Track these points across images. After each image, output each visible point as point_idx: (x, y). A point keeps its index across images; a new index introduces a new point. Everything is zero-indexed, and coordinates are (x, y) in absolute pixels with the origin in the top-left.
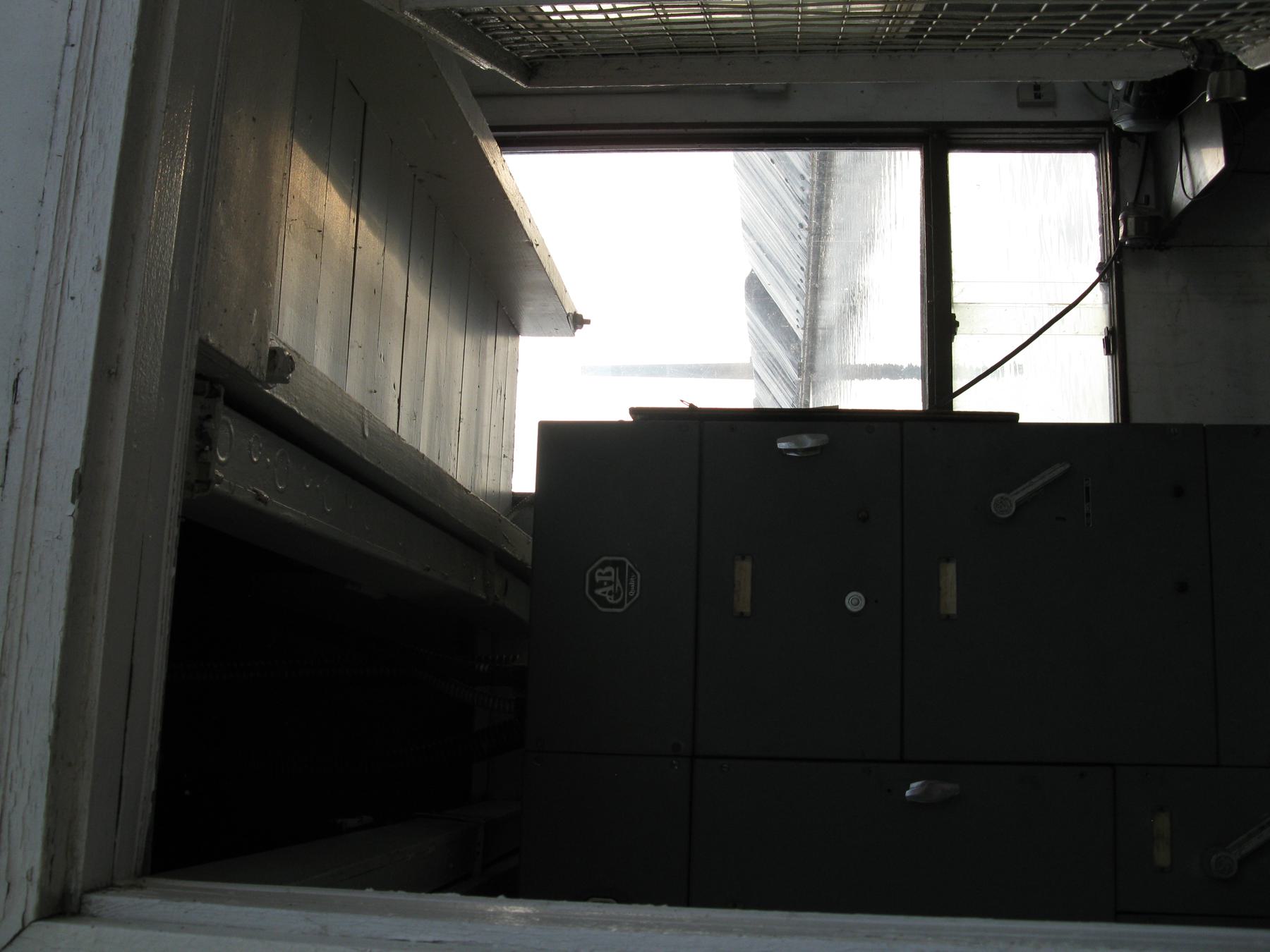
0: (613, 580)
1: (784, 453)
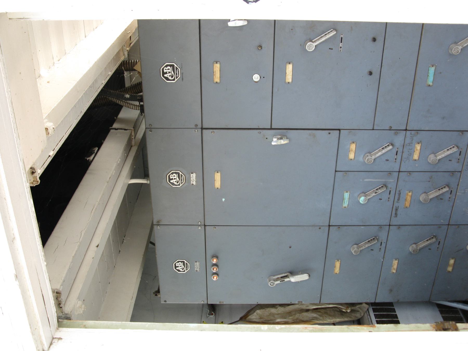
0: (176, 178)
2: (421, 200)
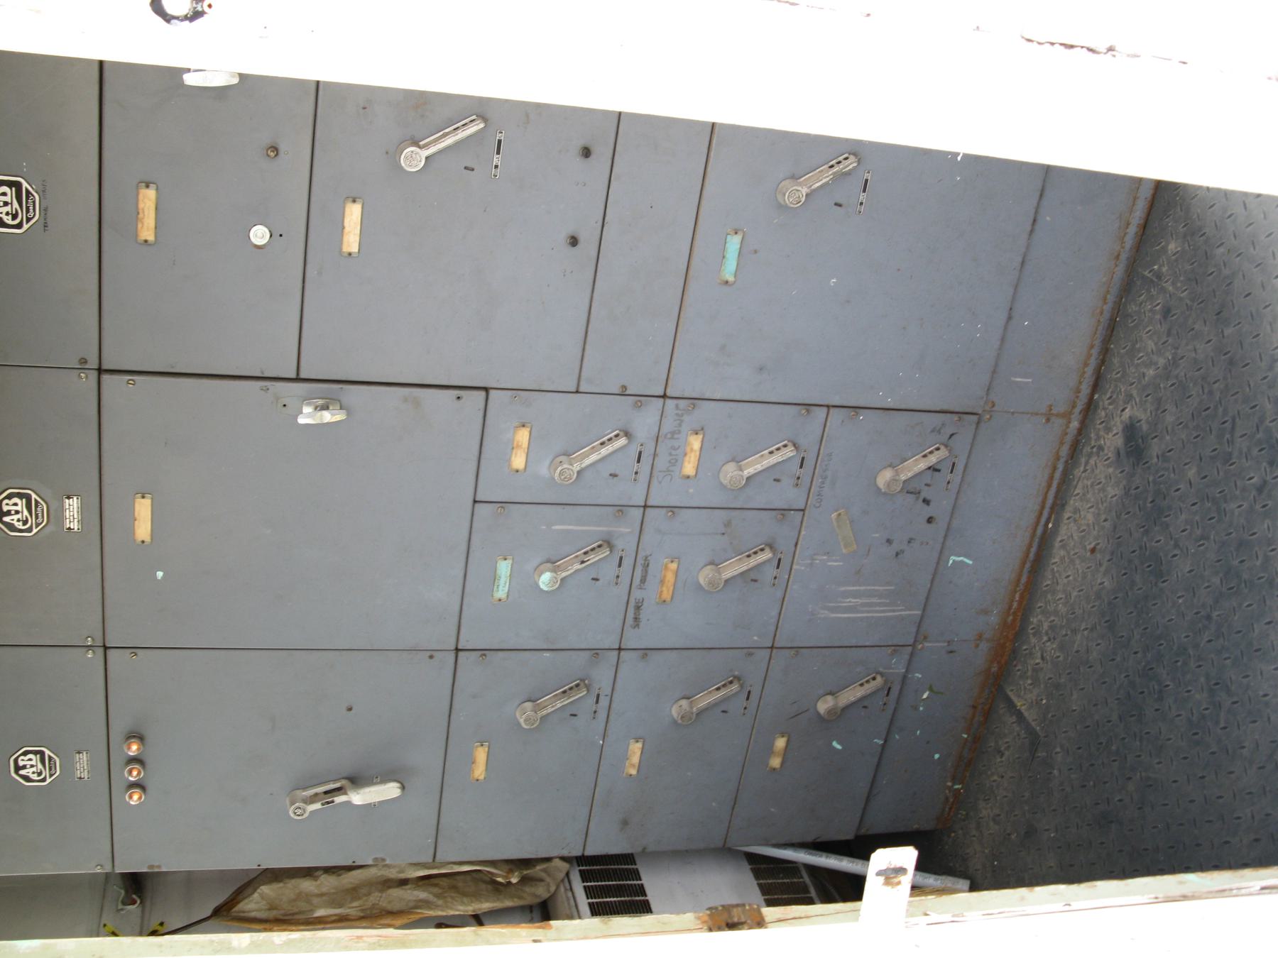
0: (10, 202)
2: (702, 581)
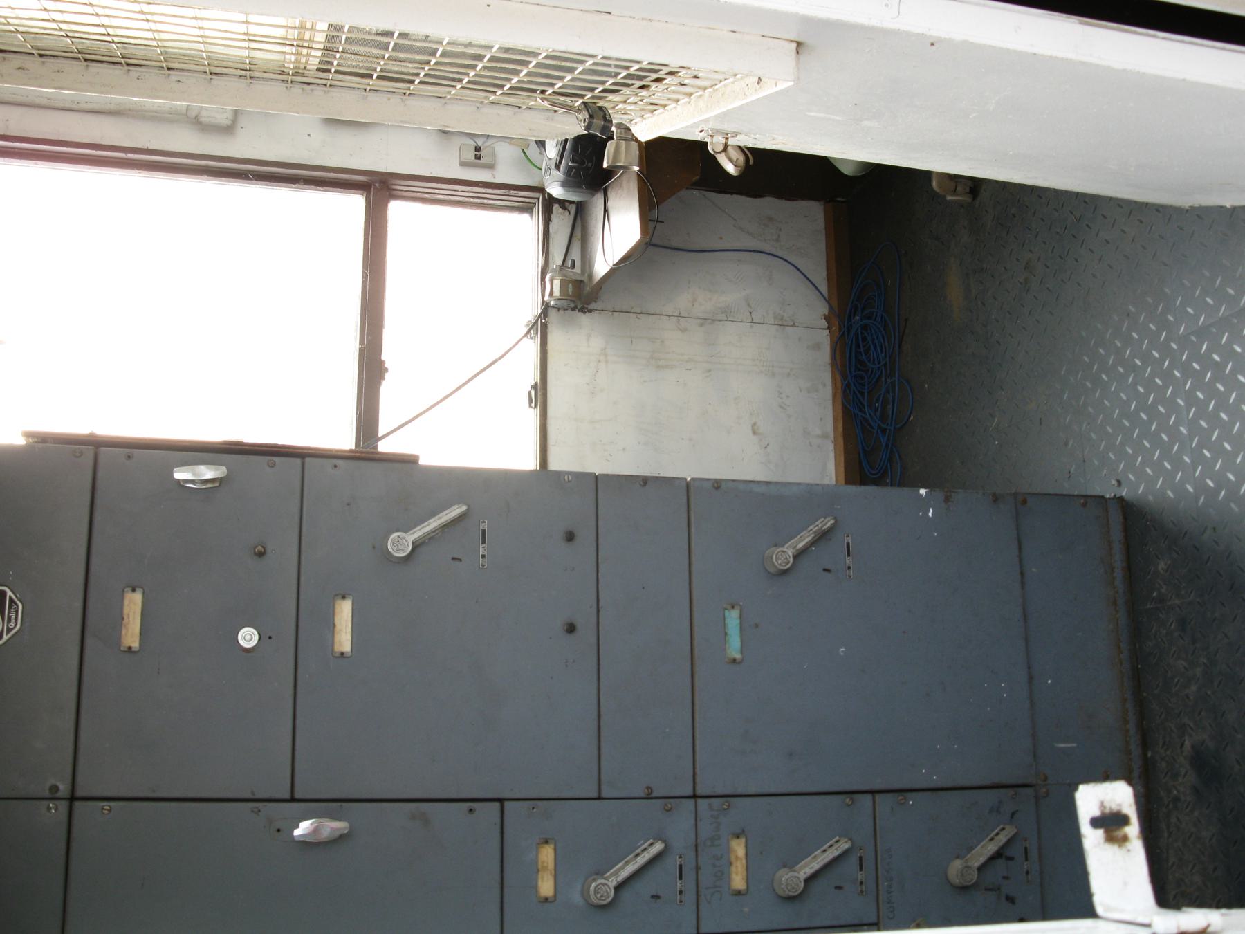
1: (182, 483)
